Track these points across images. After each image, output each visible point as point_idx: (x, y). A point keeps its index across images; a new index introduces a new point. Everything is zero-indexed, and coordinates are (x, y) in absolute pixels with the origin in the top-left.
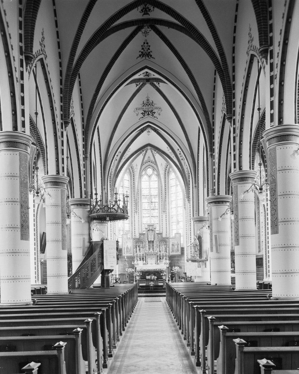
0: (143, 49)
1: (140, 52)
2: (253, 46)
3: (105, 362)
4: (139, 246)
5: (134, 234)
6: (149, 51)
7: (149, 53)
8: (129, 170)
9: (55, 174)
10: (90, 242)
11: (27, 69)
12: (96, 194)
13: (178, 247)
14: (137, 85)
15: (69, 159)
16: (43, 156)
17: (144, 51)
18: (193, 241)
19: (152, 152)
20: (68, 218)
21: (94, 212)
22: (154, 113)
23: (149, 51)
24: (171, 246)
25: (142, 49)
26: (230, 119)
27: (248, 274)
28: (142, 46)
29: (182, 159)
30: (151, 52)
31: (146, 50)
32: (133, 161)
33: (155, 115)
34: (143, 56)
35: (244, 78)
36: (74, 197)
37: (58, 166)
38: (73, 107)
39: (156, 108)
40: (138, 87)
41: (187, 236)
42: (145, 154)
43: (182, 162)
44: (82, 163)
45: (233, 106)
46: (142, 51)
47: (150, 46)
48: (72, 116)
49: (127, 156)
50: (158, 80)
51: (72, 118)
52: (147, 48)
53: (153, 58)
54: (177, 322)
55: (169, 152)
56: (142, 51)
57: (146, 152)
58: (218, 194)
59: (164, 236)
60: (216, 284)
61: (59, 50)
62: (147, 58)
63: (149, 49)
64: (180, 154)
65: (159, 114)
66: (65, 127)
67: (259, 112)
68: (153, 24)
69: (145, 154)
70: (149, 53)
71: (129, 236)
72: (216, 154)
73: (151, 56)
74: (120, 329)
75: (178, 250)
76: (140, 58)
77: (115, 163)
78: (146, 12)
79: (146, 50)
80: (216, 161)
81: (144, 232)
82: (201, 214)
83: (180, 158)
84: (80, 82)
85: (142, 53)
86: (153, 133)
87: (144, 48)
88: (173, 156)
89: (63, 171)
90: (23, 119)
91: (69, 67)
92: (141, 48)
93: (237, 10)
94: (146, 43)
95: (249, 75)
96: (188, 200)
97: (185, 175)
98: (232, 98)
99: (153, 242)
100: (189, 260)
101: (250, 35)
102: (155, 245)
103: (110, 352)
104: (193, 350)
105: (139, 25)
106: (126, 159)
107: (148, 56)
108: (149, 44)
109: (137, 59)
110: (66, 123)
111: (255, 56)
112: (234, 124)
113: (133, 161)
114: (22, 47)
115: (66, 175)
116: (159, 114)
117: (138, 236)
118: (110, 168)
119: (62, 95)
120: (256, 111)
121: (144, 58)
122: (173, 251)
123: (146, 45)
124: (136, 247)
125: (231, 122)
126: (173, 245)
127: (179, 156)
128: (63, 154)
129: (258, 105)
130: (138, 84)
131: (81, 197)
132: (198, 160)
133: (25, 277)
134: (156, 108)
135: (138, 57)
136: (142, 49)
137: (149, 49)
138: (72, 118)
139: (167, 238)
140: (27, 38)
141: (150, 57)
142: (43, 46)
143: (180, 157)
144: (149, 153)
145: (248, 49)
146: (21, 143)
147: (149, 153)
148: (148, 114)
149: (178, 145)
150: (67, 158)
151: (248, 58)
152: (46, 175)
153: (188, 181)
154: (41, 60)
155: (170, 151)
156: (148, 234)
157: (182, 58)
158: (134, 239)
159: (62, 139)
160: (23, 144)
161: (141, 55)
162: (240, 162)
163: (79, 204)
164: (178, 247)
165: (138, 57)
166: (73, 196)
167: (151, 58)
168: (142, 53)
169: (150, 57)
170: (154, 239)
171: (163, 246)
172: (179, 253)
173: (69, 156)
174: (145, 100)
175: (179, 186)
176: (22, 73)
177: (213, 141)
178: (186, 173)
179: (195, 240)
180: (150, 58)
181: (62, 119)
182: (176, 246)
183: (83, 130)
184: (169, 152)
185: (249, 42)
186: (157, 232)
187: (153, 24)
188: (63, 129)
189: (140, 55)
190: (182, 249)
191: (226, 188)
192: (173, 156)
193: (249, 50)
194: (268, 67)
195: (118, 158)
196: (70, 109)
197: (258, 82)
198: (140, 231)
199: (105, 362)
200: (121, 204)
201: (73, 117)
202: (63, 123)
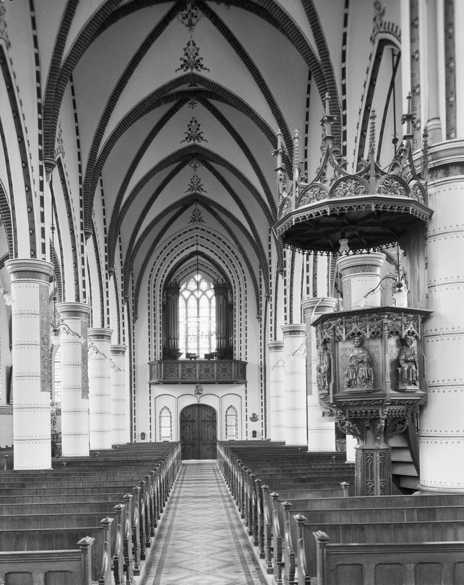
0: (192, 182)
1: (186, 133)
2: (383, 23)
3: (142, 552)
6: (198, 132)
7: (198, 61)
9: (74, 301)
15: (56, 231)
16: (58, 280)
17: (192, 132)
20: (55, 335)
25: (185, 55)
27: (73, 433)
28: (185, 49)
30: (202, 59)
31: (194, 131)
34: (190, 139)
35: (365, 86)
38: (62, 141)
46: (186, 58)
47: (198, 49)
48: (60, 155)
51: (59, 159)
52: (194, 53)
53: (205, 69)
54: (236, 501)
56: (186, 58)
61: (34, 32)
62: (198, 223)
63: (198, 129)
66: (87, 239)
70: (198, 61)
73: (202, 221)
74: (161, 505)
76: (187, 141)
79: (194, 131)
82: (297, 320)
85: (185, 61)
86: (202, 171)
87: (189, 52)
89: (44, 252)
90: (84, 290)
91: (129, 251)
92: (184, 53)
93: (308, 106)
94: (193, 121)
95: (374, 83)
98: (340, 124)
101: (378, 6)
103: (148, 541)
104: (263, 551)
107: (197, 68)
108: (197, 46)
109: (176, 71)
110: (49, 166)
114: (41, 150)
115: (48, 259)
119: (81, 198)
123: (194, 124)
128: (43, 220)
129: (393, 134)
133: (30, 437)
135: (179, 69)
136: (185, 55)
137: (198, 129)
138: (59, 159)
140: (48, 139)
141: (199, 68)
145: (374, 31)
146: (42, 273)
151: (374, 49)
152: (14, 259)
153: (268, 262)
159: (82, 256)
160: (44, 273)
163: (100, 335)
165: (179, 69)
166: (62, 297)
167: (201, 70)
168: (185, 61)
169: (199, 68)
173: (55, 226)
177: (343, 128)
180: (199, 71)
181: (41, 159)
183: (81, 186)
185: (375, 20)
188: (43, 176)
189: (191, 221)
193: (375, 33)
196: (54, 144)
199: (142, 552)
201: (62, 159)
202: (42, 166)
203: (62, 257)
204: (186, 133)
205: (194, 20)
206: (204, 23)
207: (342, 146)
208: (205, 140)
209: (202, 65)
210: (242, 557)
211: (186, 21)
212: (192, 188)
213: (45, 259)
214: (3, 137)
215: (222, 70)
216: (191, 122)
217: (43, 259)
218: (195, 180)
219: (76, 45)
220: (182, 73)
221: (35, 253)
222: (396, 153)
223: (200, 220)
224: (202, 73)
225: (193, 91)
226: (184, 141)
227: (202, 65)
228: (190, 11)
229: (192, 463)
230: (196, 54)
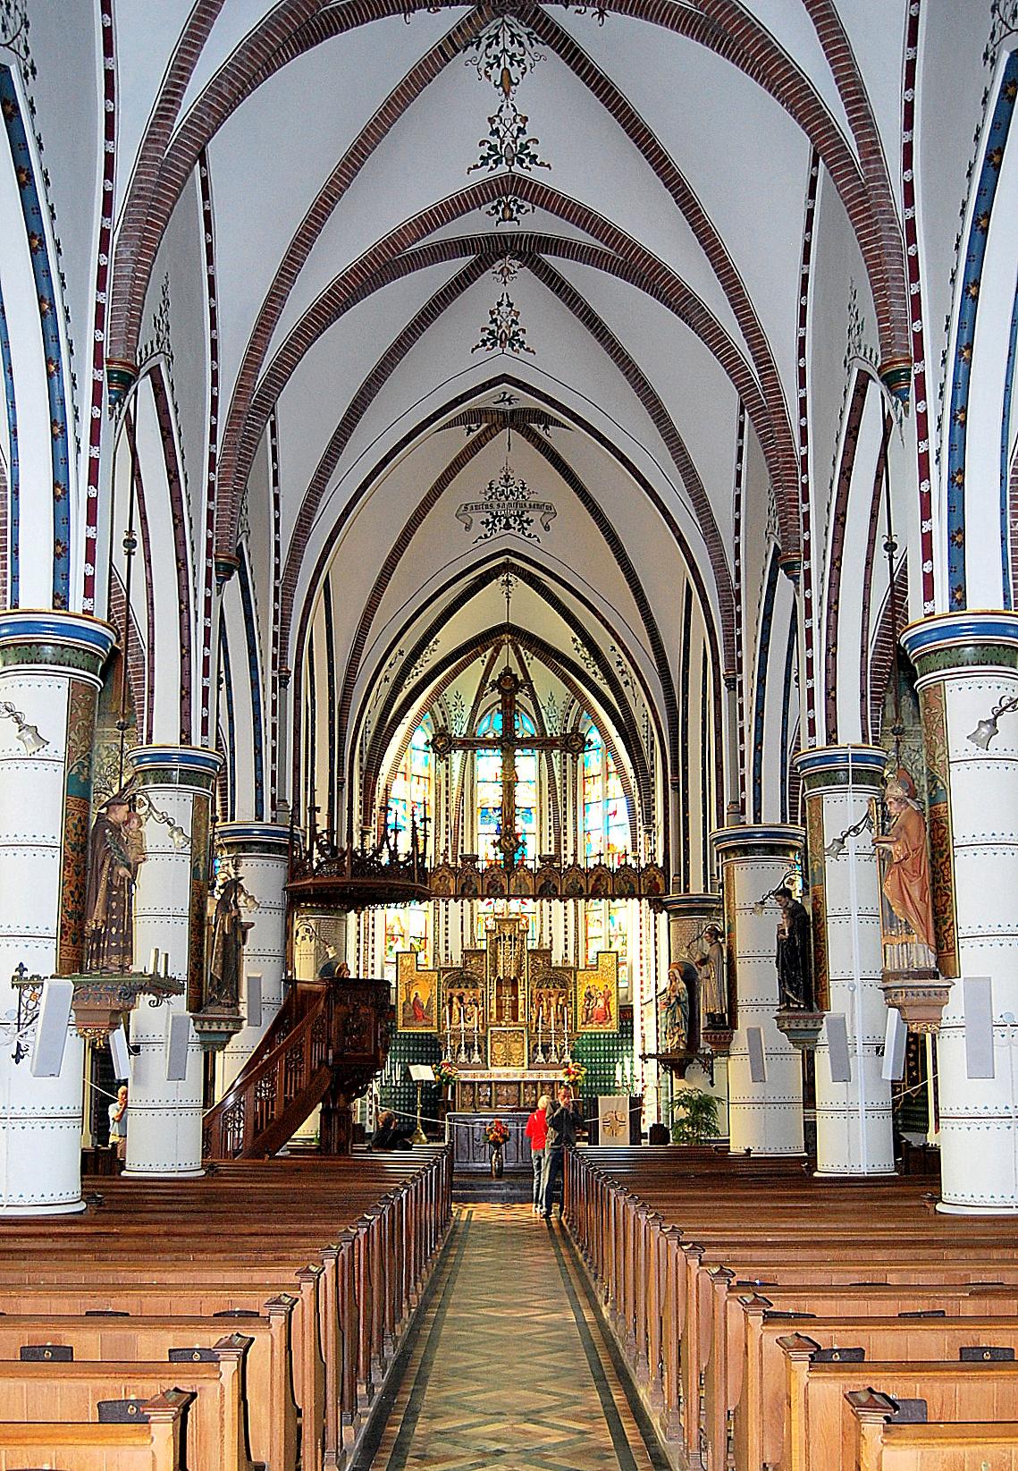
0: (495, 132)
1: (483, 330)
4: (460, 999)
5: (442, 951)
6: (522, 139)
8: (432, 714)
10: (290, 982)
11: (111, 412)
12: (314, 810)
13: (607, 1004)
14: (470, 430)
15: (223, 686)
18: (664, 983)
19: (517, 651)
21: (305, 873)
22: (528, 522)
23: (522, 139)
24: (581, 1001)
26: (790, 568)
28: (492, 313)
29: (626, 683)
32: (445, 683)
33: (530, 529)
34: (494, 344)
36: (233, 819)
37: (186, 714)
39: (537, 506)
40: (473, 435)
41: (644, 962)
42: (493, 659)
43: (627, 691)
44: (267, 697)
45: (909, 313)
49: (425, 670)
50: (547, 421)
52: (515, 127)
55: (579, 656)
56: (495, 141)
57: (497, 651)
58: (757, 819)
59: (557, 959)
60: (749, 1151)
62: (508, 349)
64: (619, 664)
65: (547, 528)
67: (891, 557)
68: (530, 251)
69: (493, 659)
71: (426, 959)
72: (748, 678)
75: (606, 1017)
77: (383, 689)
78: (508, 214)
80: (749, 701)
81: (483, 945)
83: (621, 679)
84: (205, 181)
85: (491, 333)
86: (520, 586)
88: (591, 670)
96: (648, 831)
97: (640, 751)
99: (514, 983)
100: (651, 1056)
102: (521, 997)
105: (487, 252)
106: (421, 675)
107: (512, 346)
111: (870, 377)
112: (808, 586)
113: (445, 683)
116: (547, 528)
117: (457, 960)
118: (362, 712)
120: (880, 553)
121: (498, 349)
122: (588, 1019)
124: (451, 1001)
125: (795, 579)
126: (589, 996)
127: (616, 670)
130: (473, 426)
131: (259, 816)
132: (685, 691)
134: (537, 506)
137: (521, 130)
139: (568, 970)
142: (163, 327)
143: (618, 676)
144: (507, 659)
147: (507, 659)
148: (508, 526)
149: (614, 634)
150: (220, 681)
154: (155, 373)
155: (585, 652)
156: (495, 953)
157: (666, 158)
158: (446, 970)
161: (490, 156)
162: (831, 716)
164: (607, 1004)
168: (491, 333)
170: (520, 972)
171: (553, 1000)
172: (613, 1026)
173: (139, 538)
174: (497, 477)
175: (613, 776)
176: (96, 424)
178: (642, 732)
179: (672, 978)
182: (601, 1002)
184: (579, 656)
186: (530, 946)
187: (530, 251)
190: (626, 1013)
191: (783, 798)
192: (591, 670)
194: (911, 423)
195: (393, 674)
197: (883, 456)
198: (467, 940)
200: (404, 846)
203: (151, 624)
204: (483, 330)
205: (515, 72)
206: (545, 78)
207: (910, 334)
208: (542, 164)
209: (535, 157)
210: (608, 1404)
211: (496, 73)
212: (493, 155)
213: (91, 613)
214: (6, 345)
215: (585, 165)
216: (500, 304)
217: (85, 612)
218: (508, 130)
219: (203, 105)
220: (483, 174)
221: (189, 737)
222: (892, 575)
223: (513, 340)
224: (536, 174)
225: (511, 234)
226: (476, 167)
227: (535, 157)
228: (505, 51)
229: (24, 1246)
230: (521, 130)
